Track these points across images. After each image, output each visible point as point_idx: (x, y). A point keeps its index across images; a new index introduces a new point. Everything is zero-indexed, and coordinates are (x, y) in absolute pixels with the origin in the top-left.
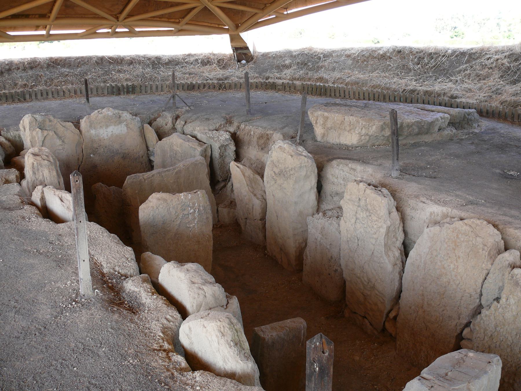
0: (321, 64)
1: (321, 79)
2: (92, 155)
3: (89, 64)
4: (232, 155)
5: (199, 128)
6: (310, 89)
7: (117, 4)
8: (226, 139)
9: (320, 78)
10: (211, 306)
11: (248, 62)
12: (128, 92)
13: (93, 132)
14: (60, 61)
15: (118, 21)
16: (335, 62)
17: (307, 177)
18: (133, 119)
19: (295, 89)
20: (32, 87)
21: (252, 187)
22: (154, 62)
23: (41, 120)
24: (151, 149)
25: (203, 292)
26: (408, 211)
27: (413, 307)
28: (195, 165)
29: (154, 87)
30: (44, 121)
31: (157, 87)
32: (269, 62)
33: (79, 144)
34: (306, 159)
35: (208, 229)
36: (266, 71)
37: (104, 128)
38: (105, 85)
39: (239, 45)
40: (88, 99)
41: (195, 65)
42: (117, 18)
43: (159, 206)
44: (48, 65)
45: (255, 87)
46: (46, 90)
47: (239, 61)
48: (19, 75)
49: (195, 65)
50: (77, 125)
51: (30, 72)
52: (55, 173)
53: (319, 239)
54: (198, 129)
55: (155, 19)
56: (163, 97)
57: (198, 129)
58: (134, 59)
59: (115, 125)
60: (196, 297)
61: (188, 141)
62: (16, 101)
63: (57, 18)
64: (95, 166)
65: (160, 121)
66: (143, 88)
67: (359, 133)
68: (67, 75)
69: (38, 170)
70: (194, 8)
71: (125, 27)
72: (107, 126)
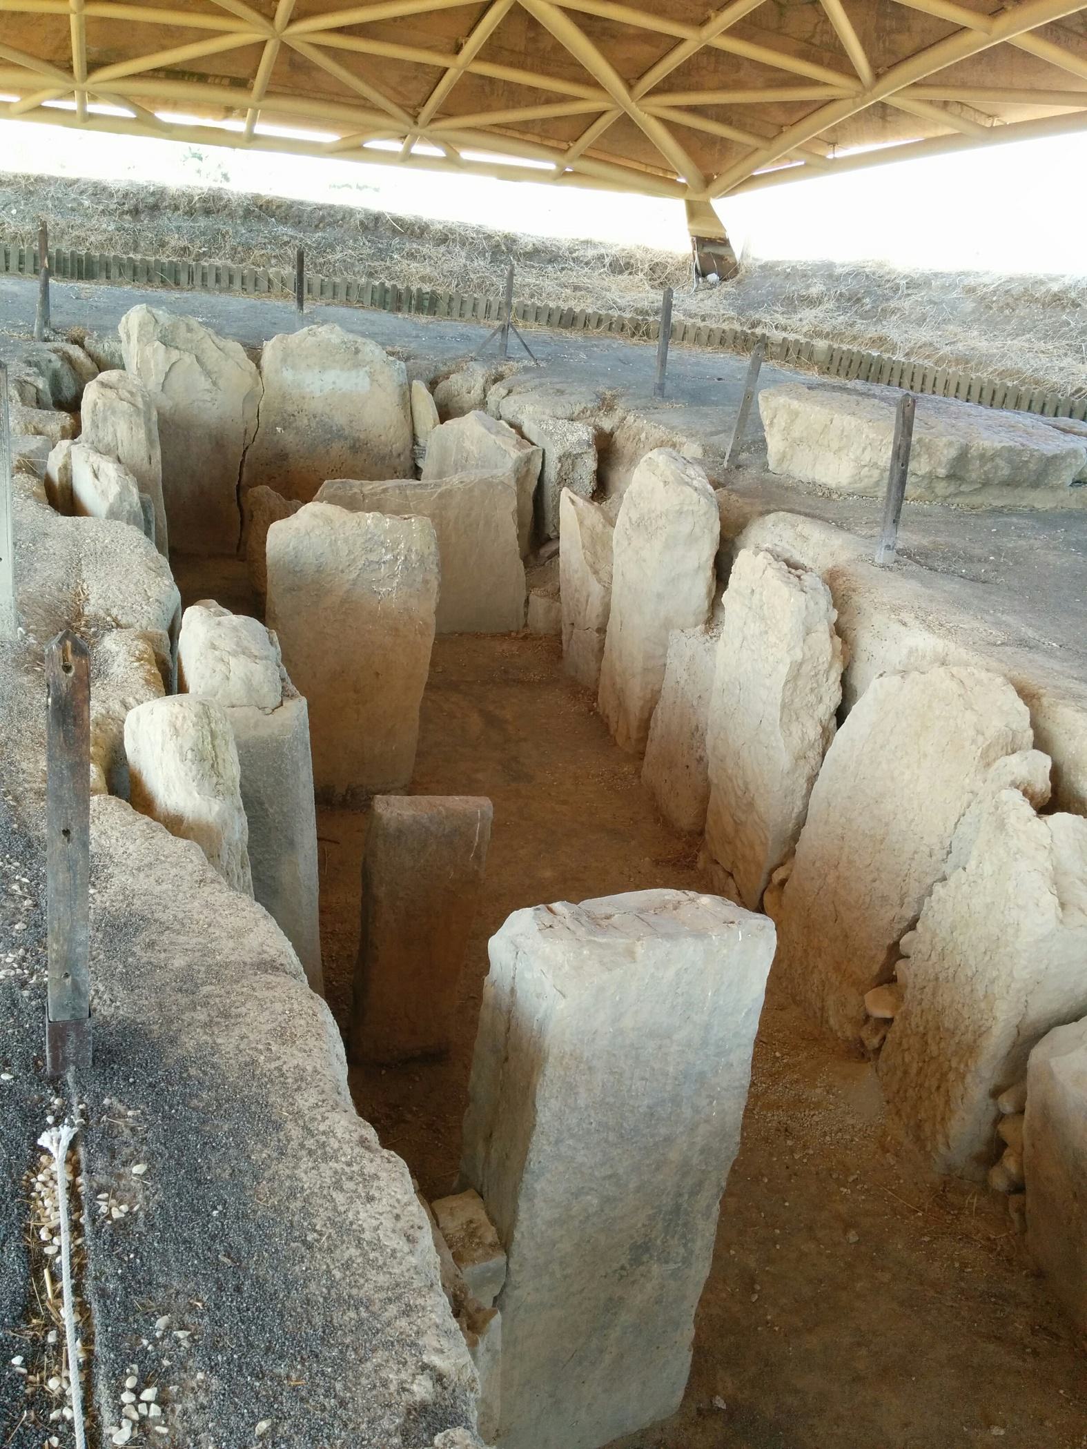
0: (893, 304)
1: (880, 341)
2: (279, 429)
3: (346, 226)
4: (587, 482)
5: (531, 409)
6: (845, 363)
7: (415, 78)
8: (579, 443)
9: (880, 339)
10: (235, 702)
11: (723, 279)
12: (420, 309)
13: (288, 375)
14: (279, 207)
15: (416, 123)
16: (931, 302)
17: (692, 539)
19: (810, 359)
20: (199, 257)
21: (595, 554)
22: (498, 246)
23: (167, 323)
24: (421, 441)
25: (224, 668)
26: (866, 641)
27: (818, 864)
28: (489, 484)
29: (482, 307)
30: (175, 326)
31: (488, 307)
32: (771, 286)
33: (250, 397)
34: (695, 494)
35: (425, 609)
36: (756, 306)
37: (316, 371)
38: (368, 283)
39: (707, 231)
41: (593, 269)
42: (415, 117)
43: (312, 530)
44: (248, 213)
45: (718, 341)
46: (230, 269)
47: (703, 274)
48: (173, 225)
49: (593, 269)
50: (255, 354)
51: (202, 222)
52: (141, 434)
53: (682, 682)
54: (530, 410)
55: (510, 133)
56: (485, 329)
57: (530, 410)
58: (452, 231)
59: (342, 369)
60: (208, 675)
61: (498, 433)
62: (157, 281)
63: (268, 93)
64: (283, 456)
65: (456, 382)
66: (456, 305)
67: (857, 460)
68: (286, 243)
69: (105, 419)
70: (603, 113)
71: (434, 141)
72: (323, 369)
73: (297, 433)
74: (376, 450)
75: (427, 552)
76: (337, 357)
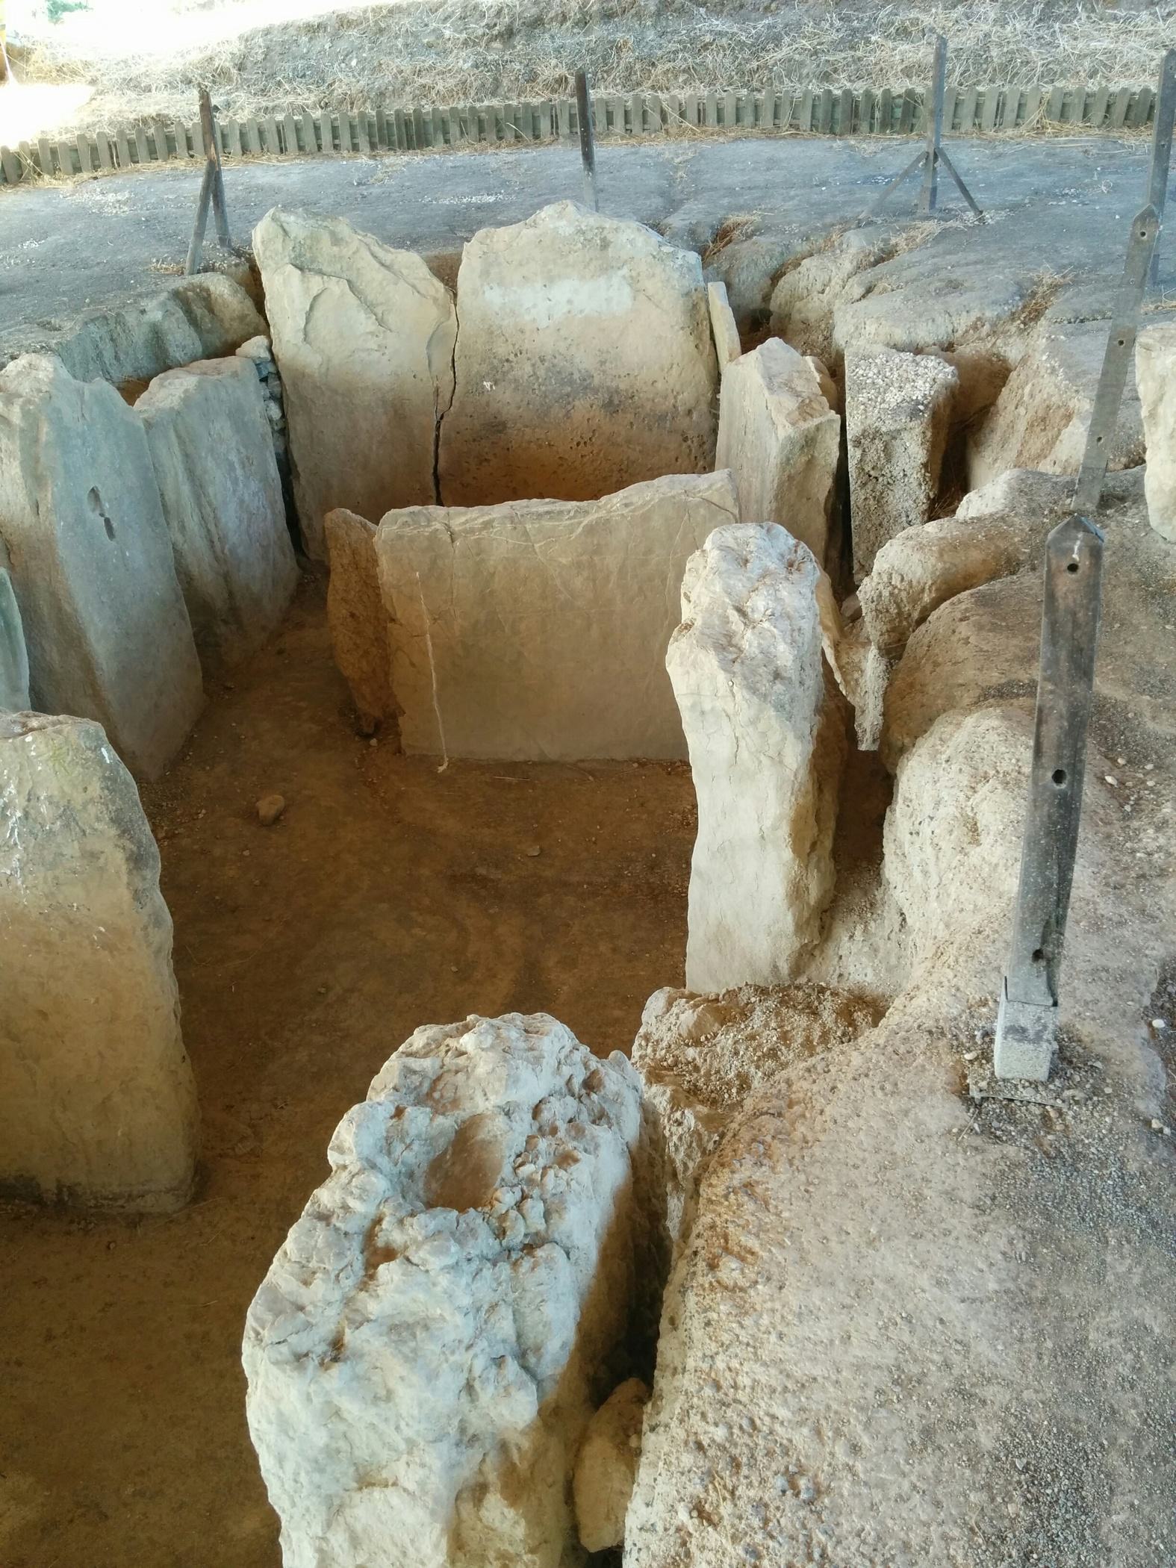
2: (487, 384)
18: (659, 258)
29: (990, 107)
30: (314, 238)
37: (539, 286)
40: (588, 156)
50: (447, 272)
59: (582, 278)
62: (509, 136)
64: (497, 426)
68: (705, 47)
72: (550, 280)
73: (516, 389)
74: (648, 406)
75: (79, 798)
76: (571, 258)
